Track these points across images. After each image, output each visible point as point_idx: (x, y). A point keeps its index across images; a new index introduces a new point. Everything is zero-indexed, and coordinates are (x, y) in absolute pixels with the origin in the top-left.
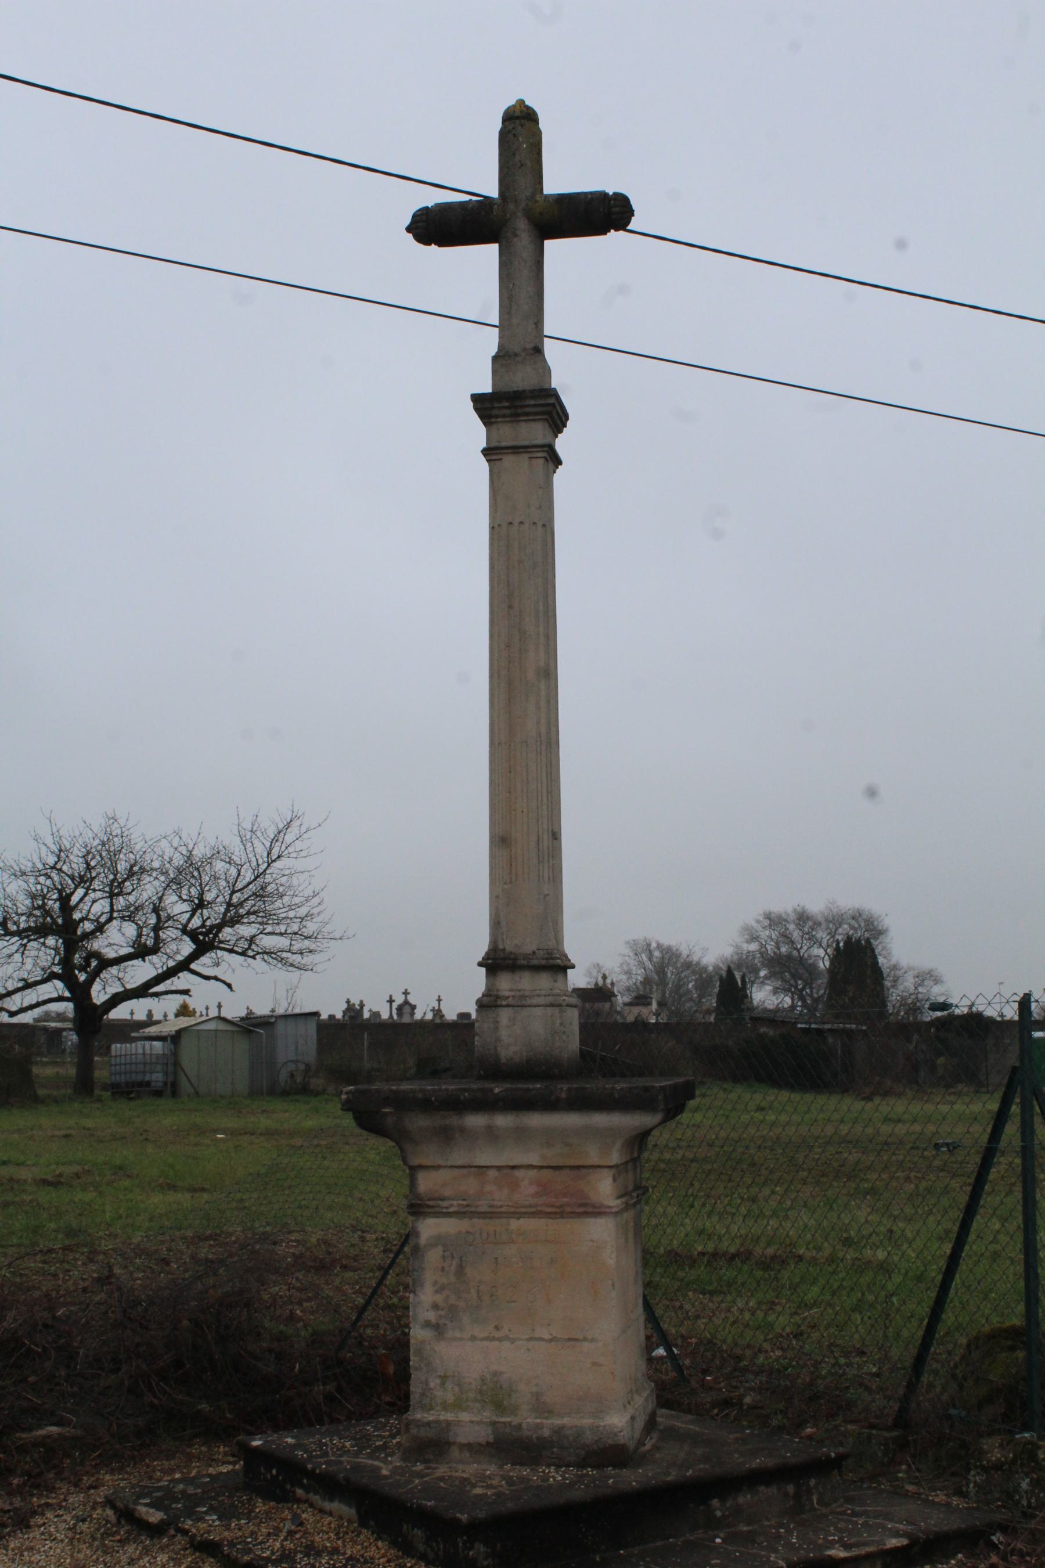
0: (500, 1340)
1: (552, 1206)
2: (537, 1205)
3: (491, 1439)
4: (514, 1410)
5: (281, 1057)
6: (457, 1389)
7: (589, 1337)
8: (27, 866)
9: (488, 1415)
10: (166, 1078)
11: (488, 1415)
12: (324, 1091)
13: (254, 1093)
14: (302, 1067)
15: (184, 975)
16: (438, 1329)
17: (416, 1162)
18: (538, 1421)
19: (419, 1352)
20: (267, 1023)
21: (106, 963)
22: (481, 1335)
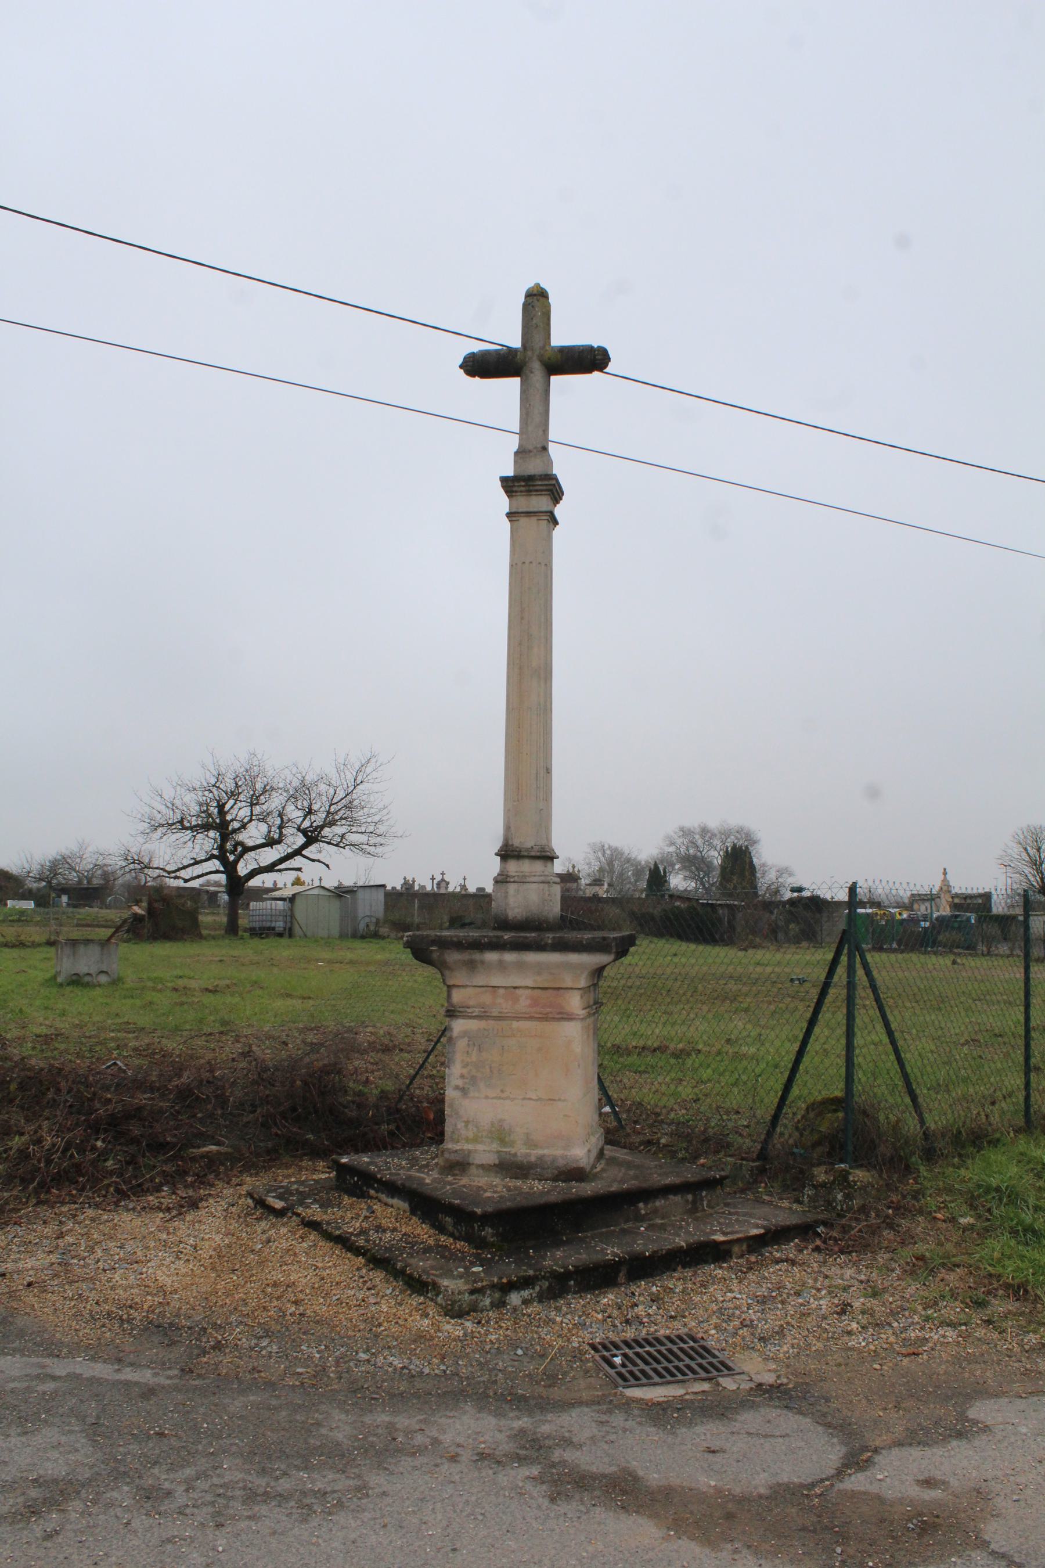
3: (497, 1162)
4: (512, 1144)
6: (475, 1129)
8: (197, 785)
9: (495, 1146)
11: (495, 1146)
13: (343, 936)
14: (374, 920)
15: (298, 858)
16: (464, 1091)
17: (451, 982)
19: (451, 1106)
20: (351, 891)
21: (247, 849)
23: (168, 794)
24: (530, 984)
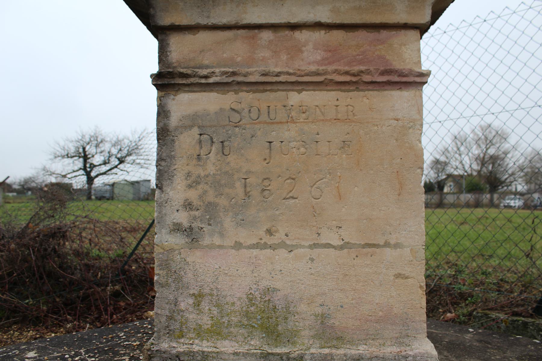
1: (347, 73)
2: (326, 73)
4: (291, 337)
8: (74, 139)
10: (110, 195)
13: (134, 200)
15: (116, 169)
16: (191, 234)
18: (326, 351)
19: (166, 265)
20: (137, 182)
21: (95, 166)
22: (250, 242)
23: (62, 143)
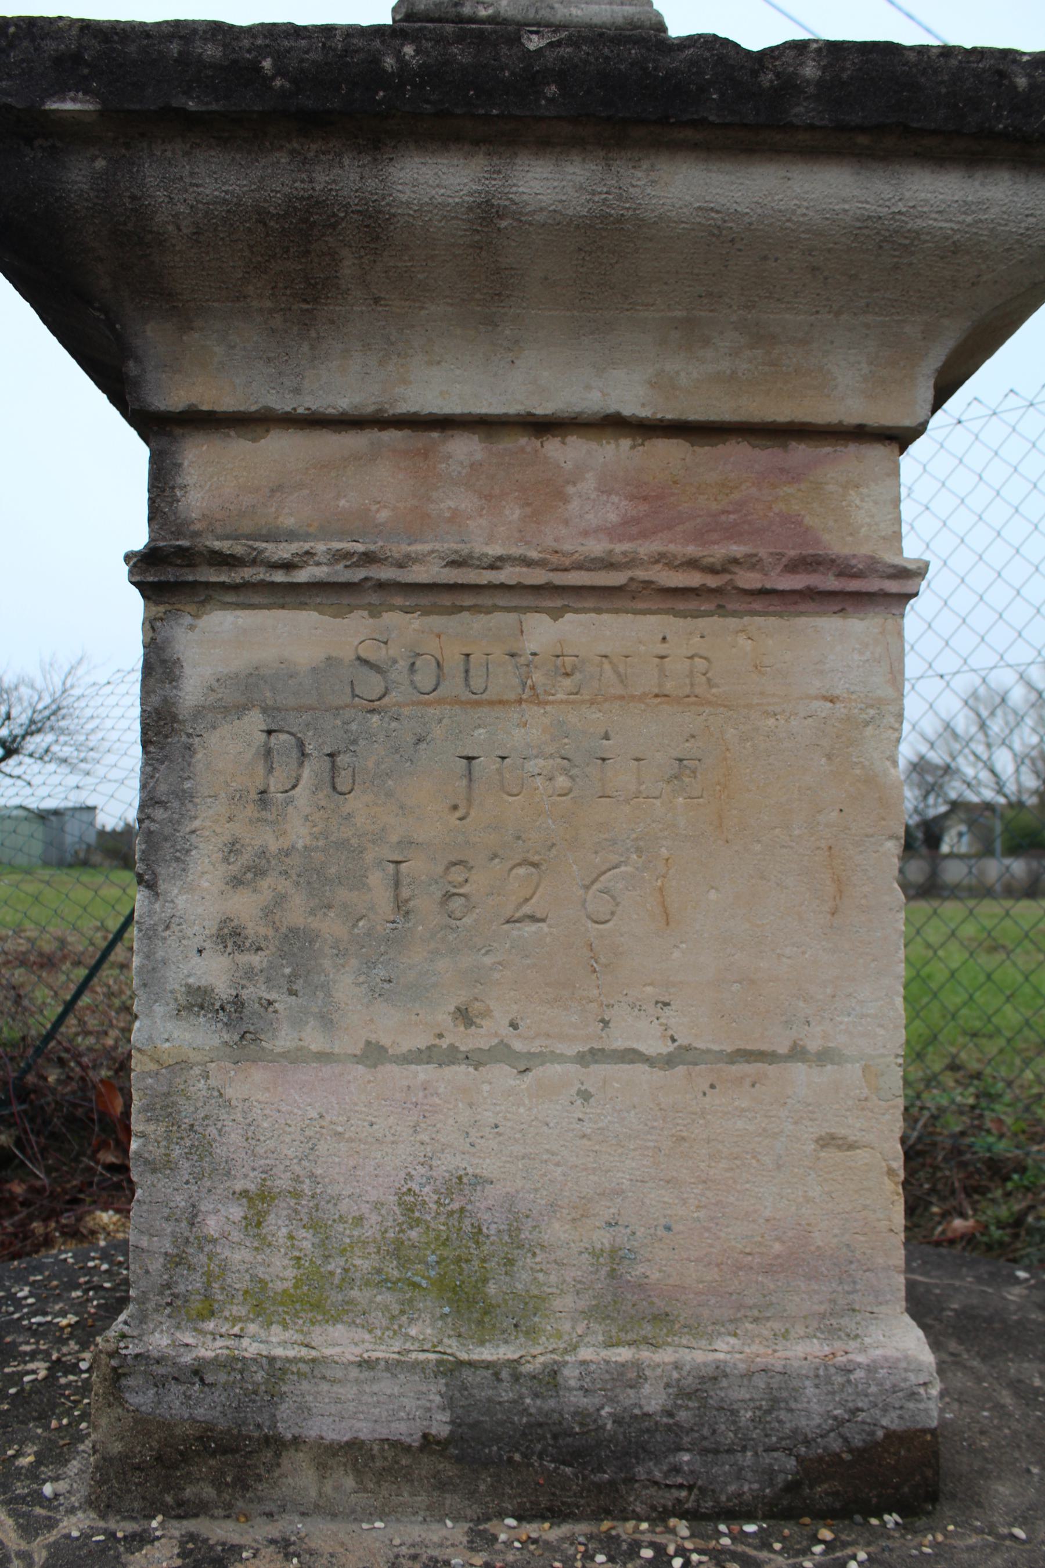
0: (475, 1059)
1: (692, 564)
2: (632, 562)
3: (440, 1426)
4: (524, 1316)
5: (69, 840)
6: (307, 1241)
7: (813, 1046)
9: (425, 1334)
11: (425, 1334)
12: (101, 865)
14: (84, 846)
16: (239, 1020)
17: (173, 396)
18: (623, 1354)
19: (165, 1108)
24: (630, 397)
